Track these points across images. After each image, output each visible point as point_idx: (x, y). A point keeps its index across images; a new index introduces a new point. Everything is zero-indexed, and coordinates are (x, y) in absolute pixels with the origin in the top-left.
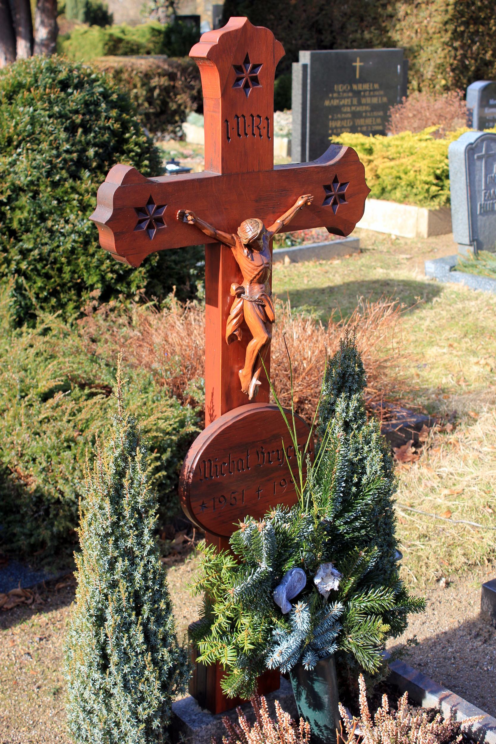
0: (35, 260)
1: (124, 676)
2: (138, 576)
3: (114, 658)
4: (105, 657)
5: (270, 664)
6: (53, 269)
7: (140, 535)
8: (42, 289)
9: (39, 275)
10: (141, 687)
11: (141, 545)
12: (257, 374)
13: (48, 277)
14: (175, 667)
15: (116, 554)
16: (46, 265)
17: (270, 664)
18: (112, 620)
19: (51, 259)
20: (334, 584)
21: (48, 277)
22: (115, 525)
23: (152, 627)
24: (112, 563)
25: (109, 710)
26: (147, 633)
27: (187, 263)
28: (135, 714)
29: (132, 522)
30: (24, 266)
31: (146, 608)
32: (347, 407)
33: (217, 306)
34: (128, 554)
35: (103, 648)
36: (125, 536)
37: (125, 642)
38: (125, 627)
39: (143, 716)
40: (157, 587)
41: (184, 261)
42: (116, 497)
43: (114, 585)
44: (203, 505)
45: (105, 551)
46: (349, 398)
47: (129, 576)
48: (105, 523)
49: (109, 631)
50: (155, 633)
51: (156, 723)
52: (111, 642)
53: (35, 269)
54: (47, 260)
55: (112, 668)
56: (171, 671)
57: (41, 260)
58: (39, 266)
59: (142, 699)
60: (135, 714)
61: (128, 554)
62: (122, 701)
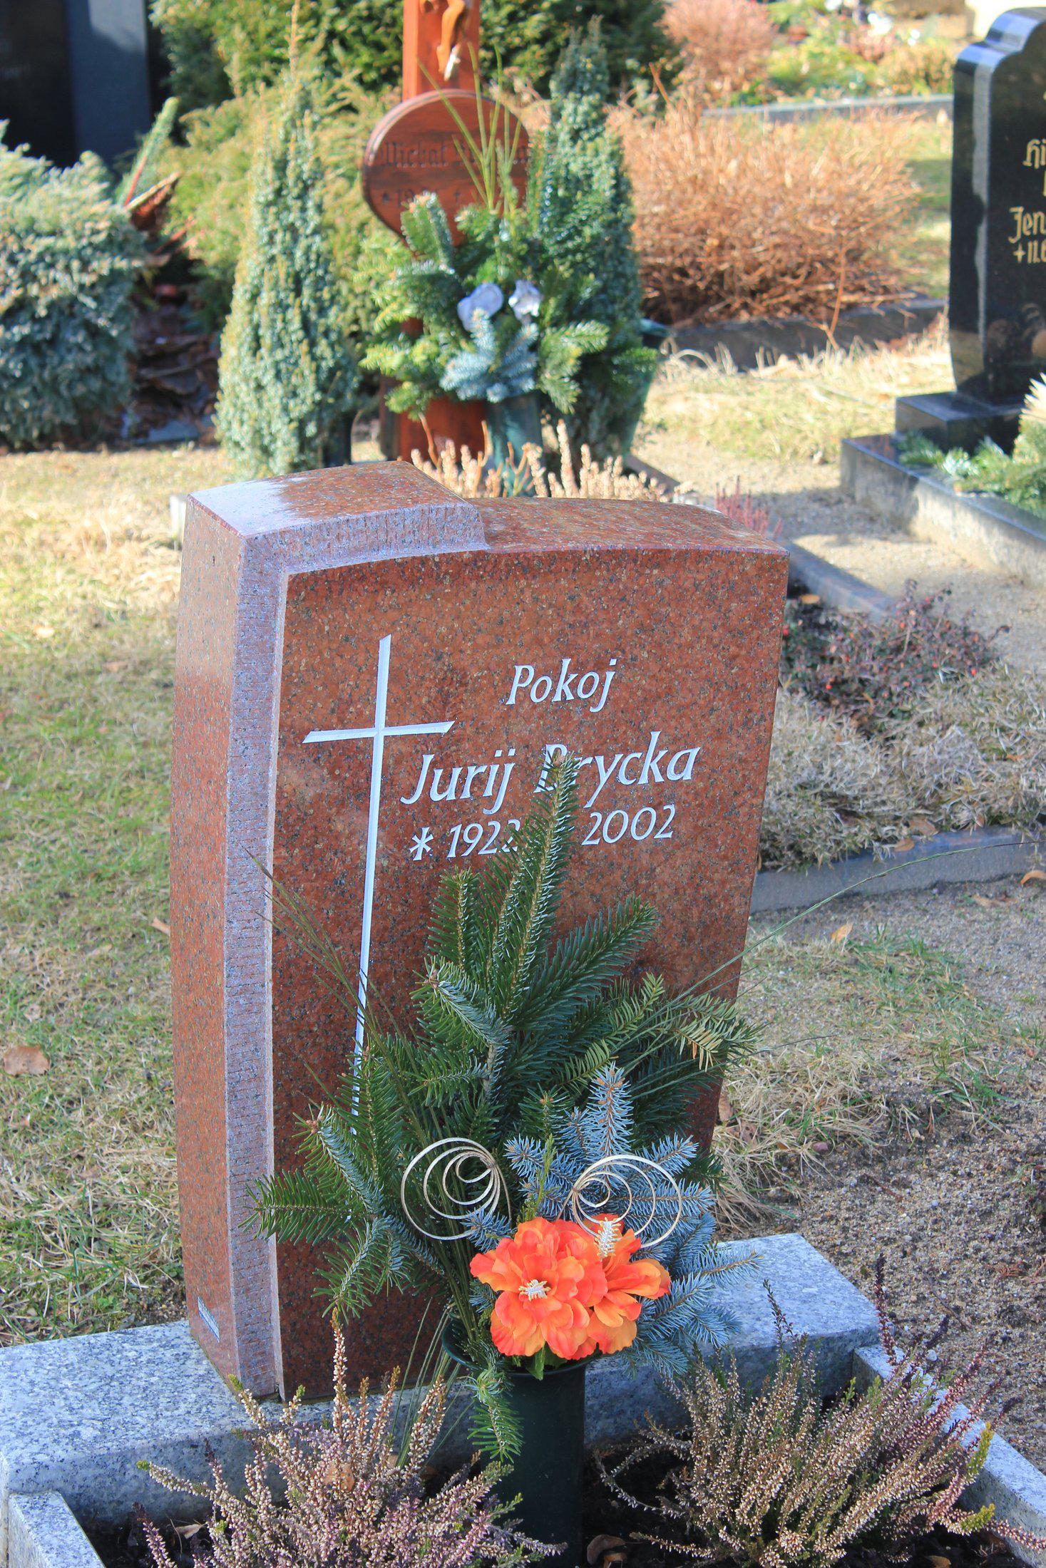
0: (360, 18)
1: (277, 363)
2: (299, 254)
3: (267, 341)
4: (257, 339)
5: (446, 384)
6: (388, 35)
7: (303, 209)
8: (368, 66)
9: (365, 42)
10: (294, 380)
11: (305, 221)
12: (456, 50)
13: (379, 47)
14: (338, 366)
15: (277, 226)
16: (377, 28)
17: (446, 384)
18: (266, 298)
19: (387, 19)
20: (533, 308)
21: (379, 47)
22: (278, 192)
23: (313, 316)
24: (271, 236)
25: (260, 405)
26: (306, 325)
27: (626, 50)
28: (285, 409)
29: (296, 192)
30: (341, 25)
31: (307, 292)
32: (575, 111)
33: (976, 331)
34: (292, 229)
35: (257, 327)
36: (288, 208)
37: (279, 325)
38: (281, 306)
39: (295, 414)
40: (320, 272)
41: (621, 47)
42: (281, 166)
43: (272, 260)
44: (385, 196)
45: (265, 224)
46: (578, 101)
47: (289, 254)
48: (268, 193)
49: (264, 310)
50: (316, 325)
51: (311, 429)
52: (265, 322)
53: (358, 33)
54: (380, 20)
55: (263, 351)
56: (332, 372)
57: (369, 18)
58: (367, 29)
59: (294, 395)
60: (285, 409)
61: (292, 229)
62: (275, 392)
